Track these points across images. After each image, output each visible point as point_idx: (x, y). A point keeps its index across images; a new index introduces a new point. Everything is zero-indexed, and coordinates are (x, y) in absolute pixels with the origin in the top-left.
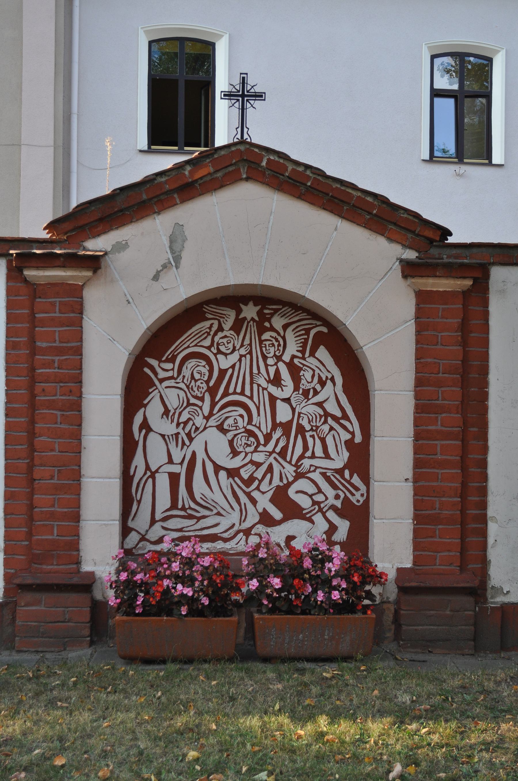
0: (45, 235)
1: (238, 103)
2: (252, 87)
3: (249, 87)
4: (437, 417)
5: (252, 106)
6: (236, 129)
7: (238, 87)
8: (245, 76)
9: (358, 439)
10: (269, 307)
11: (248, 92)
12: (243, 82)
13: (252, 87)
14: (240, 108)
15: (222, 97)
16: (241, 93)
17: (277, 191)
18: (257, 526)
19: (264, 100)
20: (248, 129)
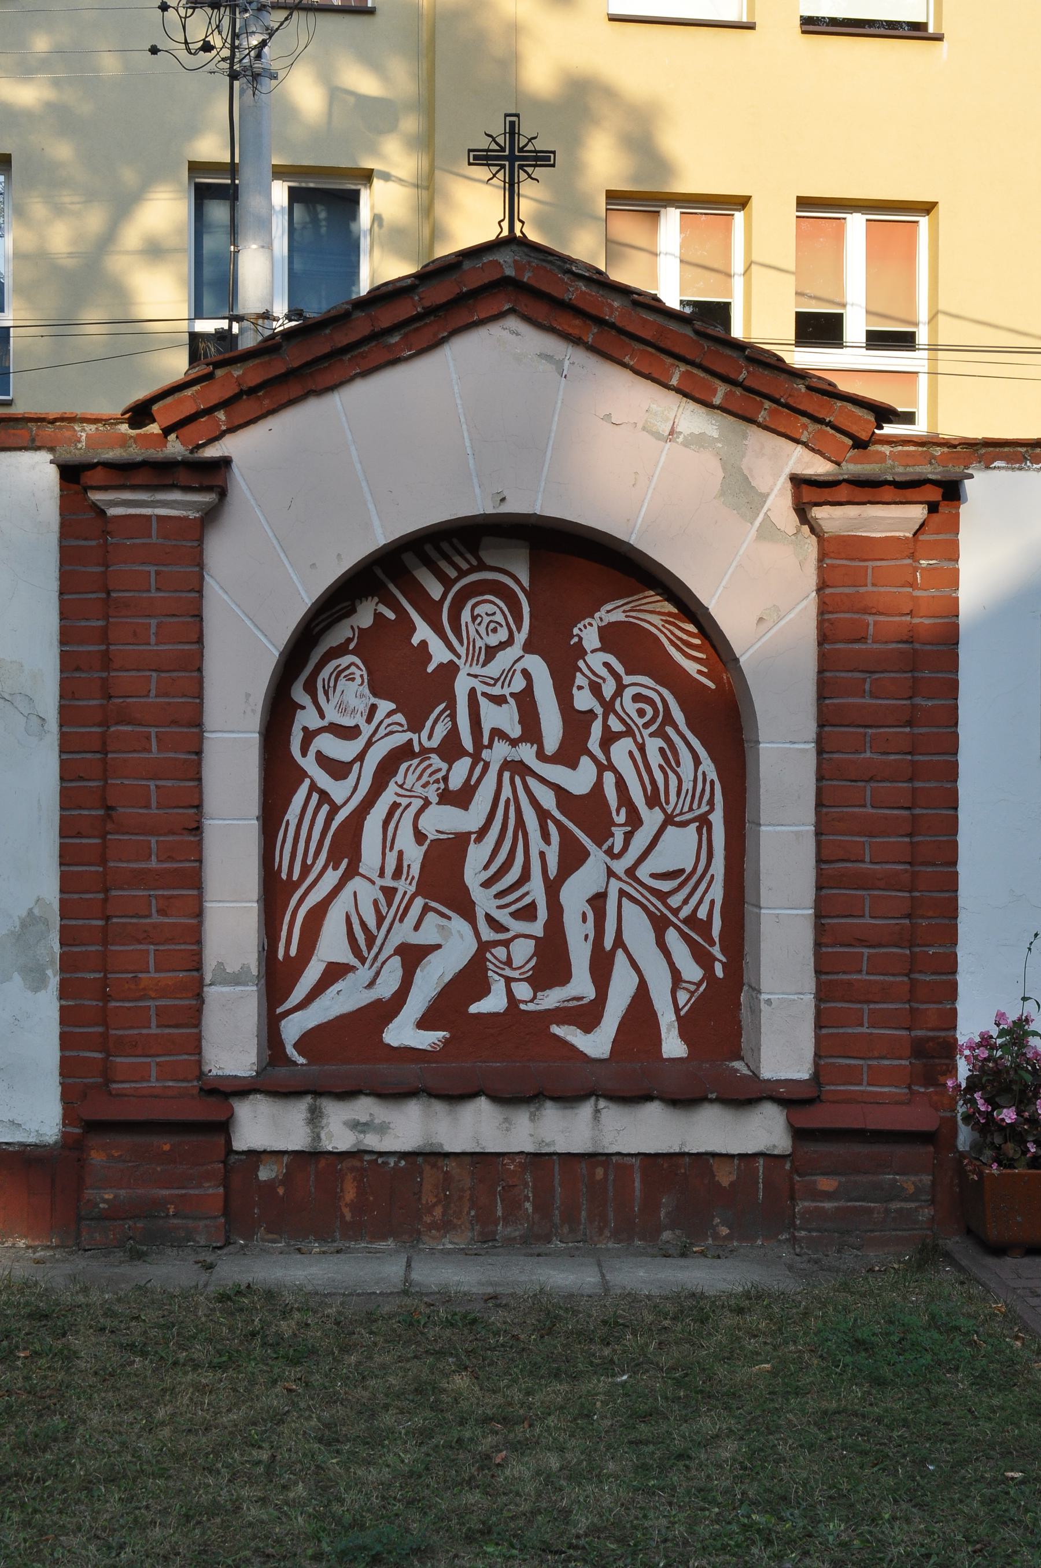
2: (530, 140)
3: (523, 141)
4: (865, 787)
6: (499, 223)
7: (523, 176)
9: (677, 819)
10: (656, 912)
12: (512, 131)
13: (530, 140)
17: (571, 344)
18: (276, 25)
20: (523, 223)
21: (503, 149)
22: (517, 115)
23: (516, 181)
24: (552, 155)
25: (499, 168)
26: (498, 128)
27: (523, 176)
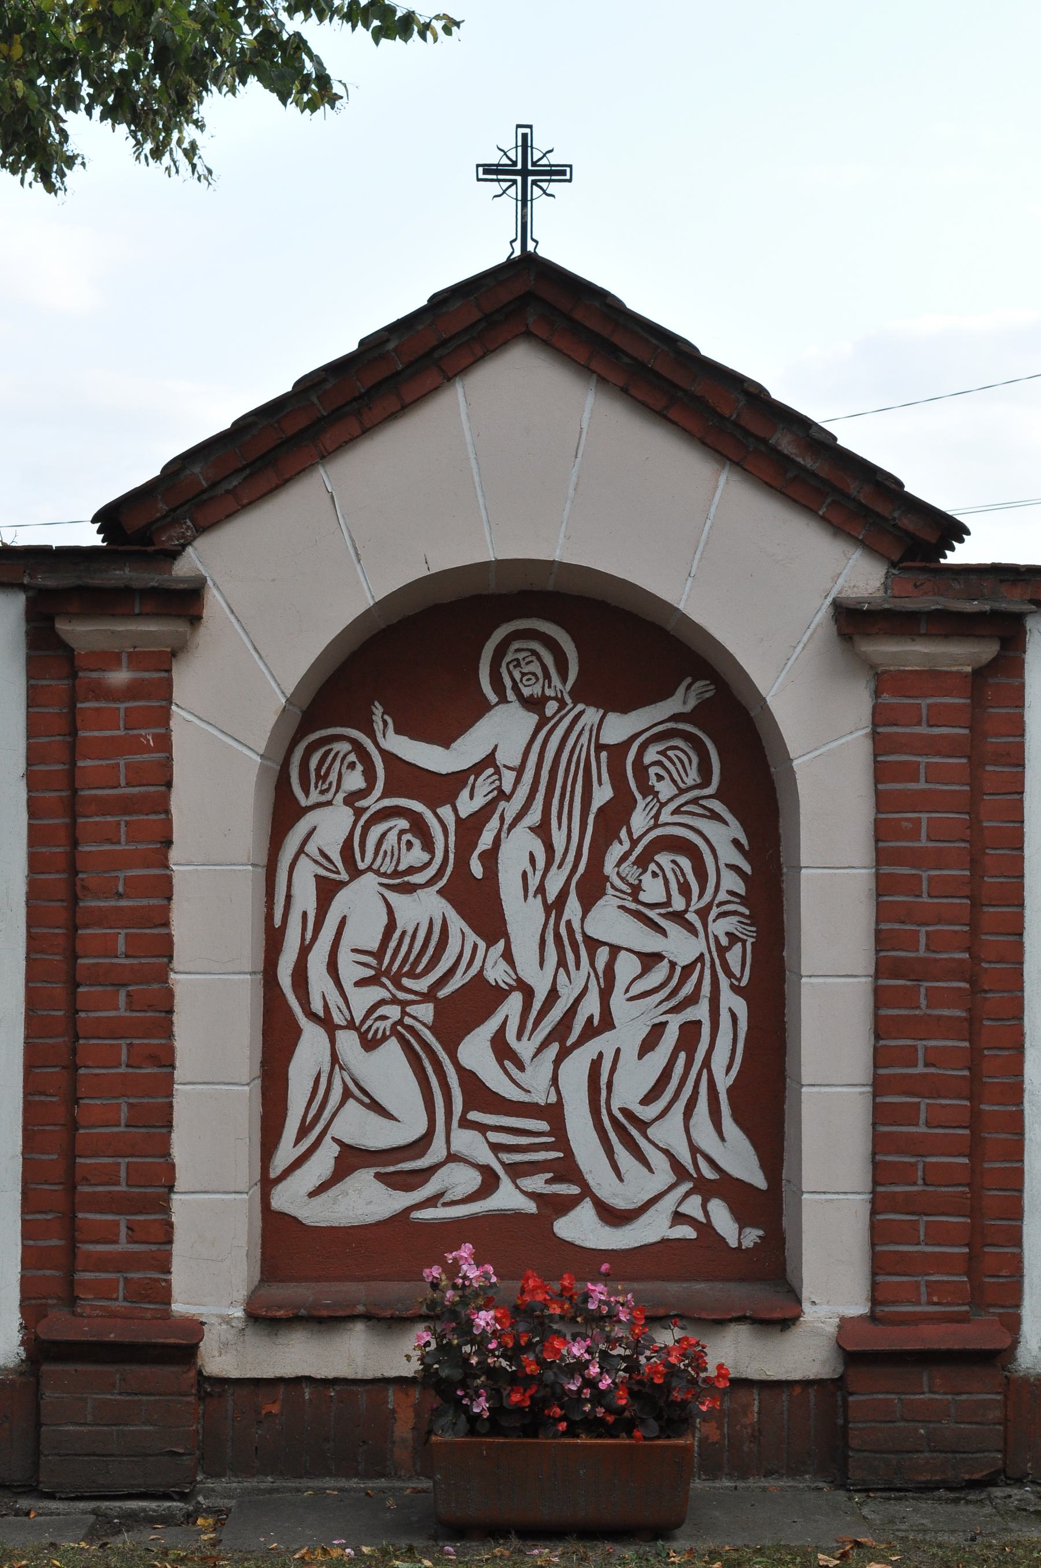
0: (91, 537)
1: (534, 160)
3: (537, 155)
5: (505, 154)
6: (512, 242)
7: (537, 191)
8: (527, 131)
11: (534, 182)
12: (525, 144)
14: (519, 198)
15: (568, 169)
16: (530, 179)
19: (570, 181)
20: (537, 242)
21: (515, 164)
22: (530, 127)
23: (529, 198)
24: (568, 169)
25: (510, 183)
26: (509, 141)
27: (537, 191)
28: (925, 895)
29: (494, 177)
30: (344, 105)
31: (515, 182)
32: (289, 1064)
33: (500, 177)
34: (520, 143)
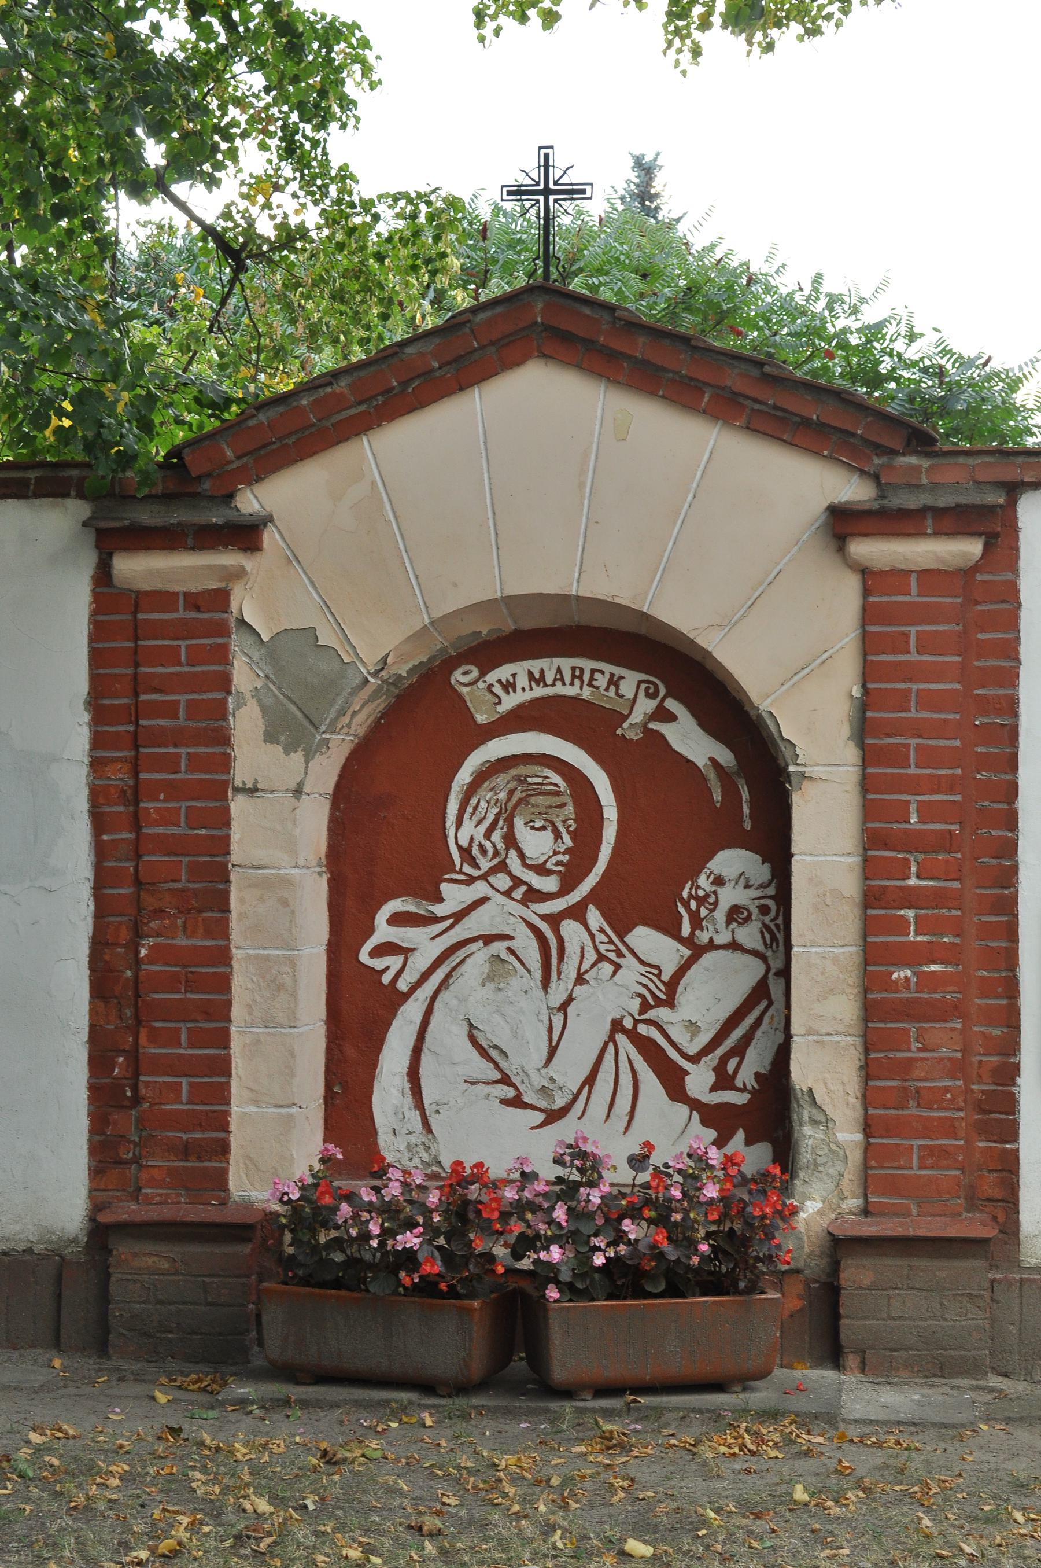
7: (535, 175)
8: (549, 151)
14: (551, 169)
16: (542, 187)
19: (503, 187)
22: (552, 147)
26: (532, 163)
28: (913, 766)
29: (575, 187)
30: (248, 87)
31: (556, 183)
32: (363, 945)
33: (570, 187)
34: (542, 163)
